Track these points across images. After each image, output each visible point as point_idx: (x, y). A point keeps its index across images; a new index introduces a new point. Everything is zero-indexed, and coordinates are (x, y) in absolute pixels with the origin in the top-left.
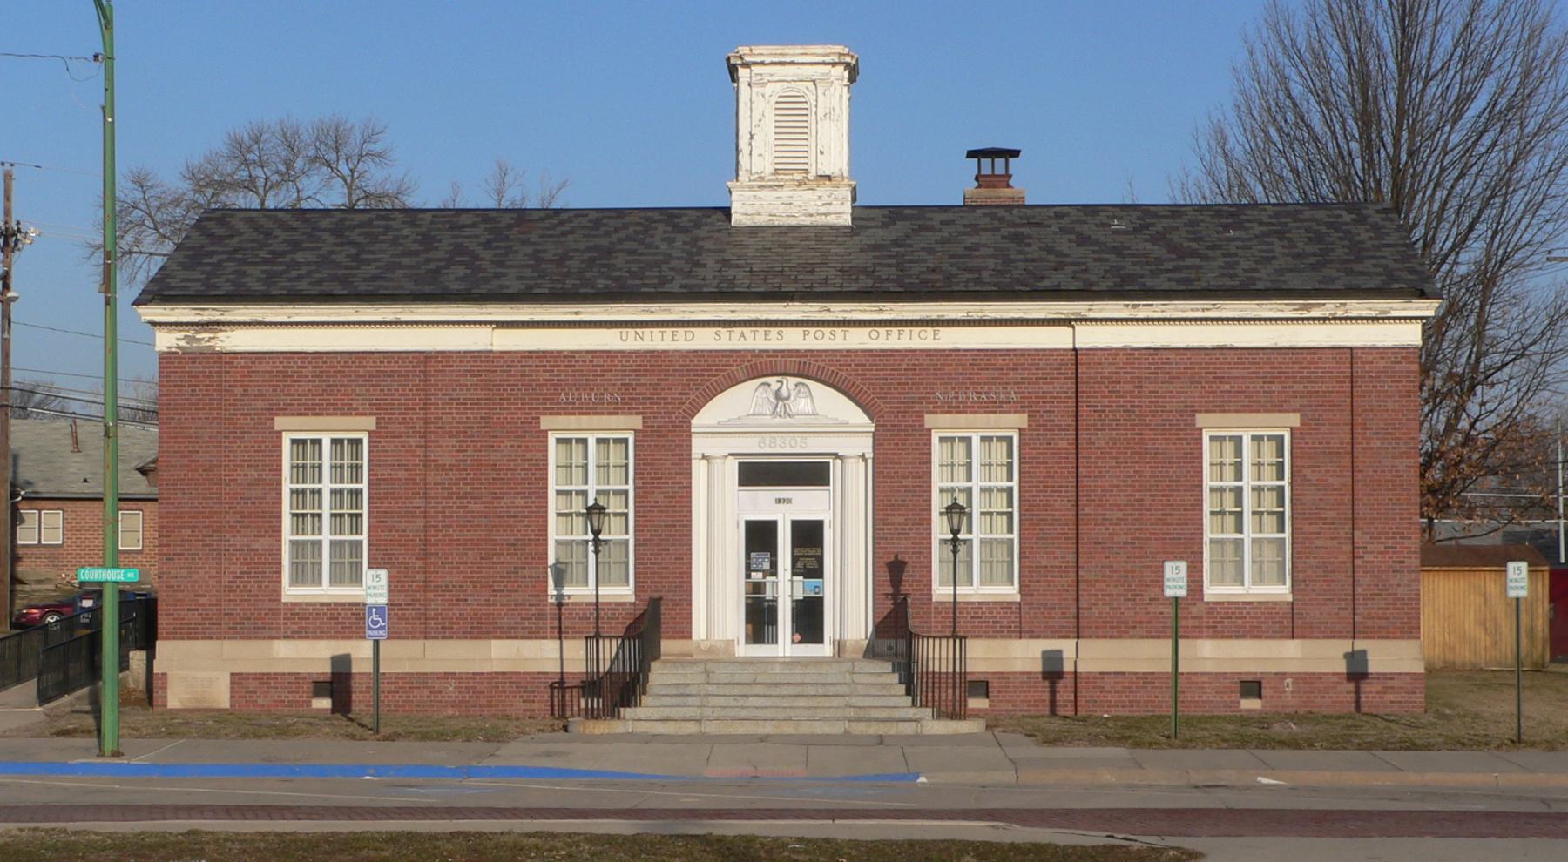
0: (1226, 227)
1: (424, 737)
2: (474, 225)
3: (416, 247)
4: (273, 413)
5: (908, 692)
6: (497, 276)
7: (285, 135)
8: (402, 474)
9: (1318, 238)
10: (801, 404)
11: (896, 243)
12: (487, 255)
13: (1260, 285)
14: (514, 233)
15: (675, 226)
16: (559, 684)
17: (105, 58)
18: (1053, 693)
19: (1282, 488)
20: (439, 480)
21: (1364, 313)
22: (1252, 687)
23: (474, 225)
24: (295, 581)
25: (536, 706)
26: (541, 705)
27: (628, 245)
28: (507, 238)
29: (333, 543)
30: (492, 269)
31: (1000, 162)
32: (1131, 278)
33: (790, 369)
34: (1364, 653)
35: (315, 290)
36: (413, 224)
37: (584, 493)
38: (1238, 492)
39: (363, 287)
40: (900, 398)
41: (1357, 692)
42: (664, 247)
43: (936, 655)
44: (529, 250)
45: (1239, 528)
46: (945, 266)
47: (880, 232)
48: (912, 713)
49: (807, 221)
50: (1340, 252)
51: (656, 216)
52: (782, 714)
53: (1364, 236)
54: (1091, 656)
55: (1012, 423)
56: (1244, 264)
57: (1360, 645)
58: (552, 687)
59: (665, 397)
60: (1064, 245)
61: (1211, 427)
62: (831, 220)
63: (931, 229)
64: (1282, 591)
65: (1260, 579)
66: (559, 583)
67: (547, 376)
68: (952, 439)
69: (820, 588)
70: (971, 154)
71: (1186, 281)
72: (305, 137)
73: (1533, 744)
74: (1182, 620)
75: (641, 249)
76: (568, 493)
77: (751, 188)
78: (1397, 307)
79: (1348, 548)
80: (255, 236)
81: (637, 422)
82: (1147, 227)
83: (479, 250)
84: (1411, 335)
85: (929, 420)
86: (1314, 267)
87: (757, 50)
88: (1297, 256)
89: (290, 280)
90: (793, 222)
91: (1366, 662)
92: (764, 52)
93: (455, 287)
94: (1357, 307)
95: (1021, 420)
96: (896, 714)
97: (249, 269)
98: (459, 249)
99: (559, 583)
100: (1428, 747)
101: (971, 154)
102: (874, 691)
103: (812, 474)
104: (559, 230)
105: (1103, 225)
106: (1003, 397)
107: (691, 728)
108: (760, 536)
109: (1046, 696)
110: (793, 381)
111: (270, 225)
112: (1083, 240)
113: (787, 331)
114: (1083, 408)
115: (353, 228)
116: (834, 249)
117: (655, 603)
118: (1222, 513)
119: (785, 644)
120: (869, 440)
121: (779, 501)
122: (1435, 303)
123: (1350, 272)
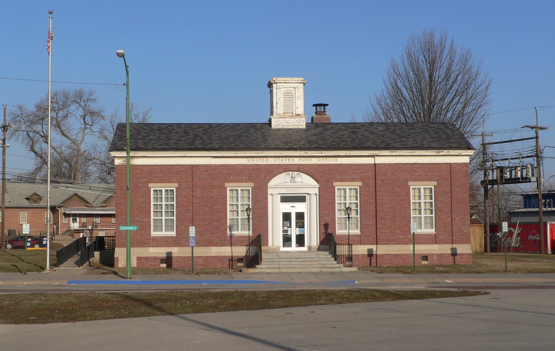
0: (410, 129)
1: (207, 273)
2: (198, 128)
3: (183, 134)
4: (148, 182)
5: (335, 260)
6: (211, 143)
7: (64, 94)
8: (186, 200)
9: (436, 133)
10: (298, 179)
11: (320, 134)
12: (205, 137)
13: (425, 146)
14: (210, 130)
15: (256, 128)
16: (231, 260)
17: (127, 85)
18: (371, 260)
19: (432, 202)
20: (196, 201)
21: (454, 154)
22: (425, 258)
23: (198, 128)
24: (154, 231)
25: (224, 265)
26: (226, 265)
27: (244, 134)
28: (209, 132)
29: (165, 219)
30: (208, 141)
31: (322, 107)
32: (389, 144)
33: (295, 169)
34: (456, 248)
35: (160, 147)
36: (180, 128)
37: (345, 204)
38: (420, 203)
39: (174, 146)
40: (326, 177)
41: (454, 259)
42: (255, 135)
43: (342, 250)
44: (217, 135)
45: (420, 214)
46: (336, 141)
47: (315, 131)
48: (337, 265)
49: (293, 127)
50: (444, 137)
51: (249, 125)
52: (302, 266)
53: (449, 132)
54: (381, 250)
55: (357, 185)
56: (419, 140)
57: (454, 246)
58: (229, 260)
59: (260, 177)
60: (367, 134)
61: (413, 185)
62: (300, 127)
63: (328, 129)
64: (358, 232)
65: (426, 228)
66: (231, 230)
67: (227, 171)
68: (341, 189)
69: (304, 231)
70: (314, 105)
71: (403, 145)
72: (71, 94)
73: (510, 271)
74: (416, 239)
75: (249, 135)
76: (233, 205)
77: (277, 118)
78: (463, 152)
79: (450, 219)
80: (136, 131)
81: (252, 184)
82: (389, 129)
83: (202, 136)
84: (466, 160)
85: (335, 184)
86: (438, 141)
87: (279, 79)
88: (432, 138)
89: (151, 144)
90: (289, 127)
91: (456, 250)
92: (280, 79)
93: (200, 146)
94: (452, 152)
95: (360, 183)
96: (333, 266)
97: (139, 141)
98: (196, 136)
99: (230, 231)
100: (483, 273)
101: (314, 105)
102: (326, 260)
103: (301, 199)
104: (223, 130)
105: (375, 128)
106: (355, 177)
107: (277, 270)
108: (287, 217)
109: (369, 261)
110: (296, 173)
111: (138, 128)
112: (372, 133)
113: (295, 159)
114: (377, 180)
115: (163, 129)
116: (303, 135)
117: (259, 235)
118: (415, 209)
119: (294, 247)
120: (318, 189)
121: (292, 207)
122: (473, 151)
123: (448, 142)
